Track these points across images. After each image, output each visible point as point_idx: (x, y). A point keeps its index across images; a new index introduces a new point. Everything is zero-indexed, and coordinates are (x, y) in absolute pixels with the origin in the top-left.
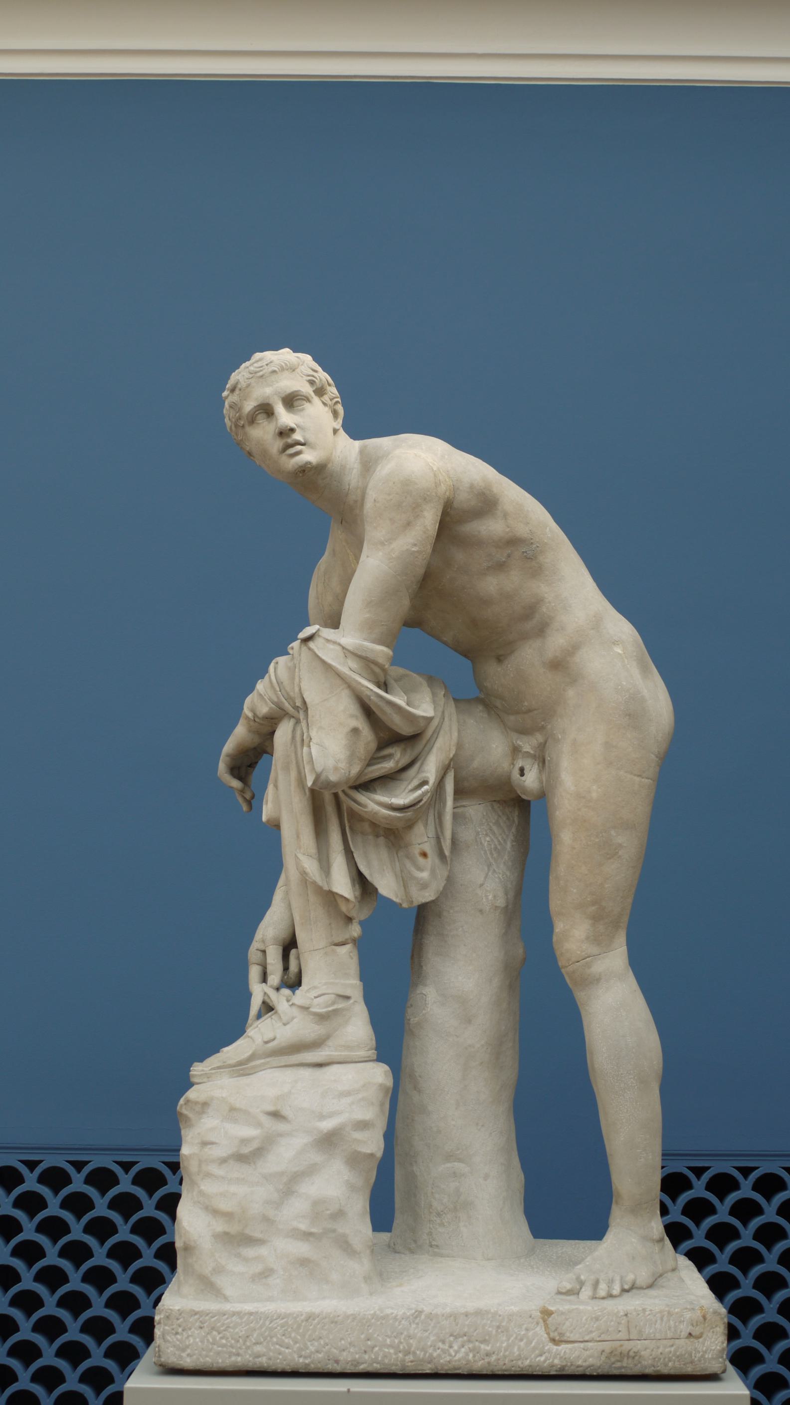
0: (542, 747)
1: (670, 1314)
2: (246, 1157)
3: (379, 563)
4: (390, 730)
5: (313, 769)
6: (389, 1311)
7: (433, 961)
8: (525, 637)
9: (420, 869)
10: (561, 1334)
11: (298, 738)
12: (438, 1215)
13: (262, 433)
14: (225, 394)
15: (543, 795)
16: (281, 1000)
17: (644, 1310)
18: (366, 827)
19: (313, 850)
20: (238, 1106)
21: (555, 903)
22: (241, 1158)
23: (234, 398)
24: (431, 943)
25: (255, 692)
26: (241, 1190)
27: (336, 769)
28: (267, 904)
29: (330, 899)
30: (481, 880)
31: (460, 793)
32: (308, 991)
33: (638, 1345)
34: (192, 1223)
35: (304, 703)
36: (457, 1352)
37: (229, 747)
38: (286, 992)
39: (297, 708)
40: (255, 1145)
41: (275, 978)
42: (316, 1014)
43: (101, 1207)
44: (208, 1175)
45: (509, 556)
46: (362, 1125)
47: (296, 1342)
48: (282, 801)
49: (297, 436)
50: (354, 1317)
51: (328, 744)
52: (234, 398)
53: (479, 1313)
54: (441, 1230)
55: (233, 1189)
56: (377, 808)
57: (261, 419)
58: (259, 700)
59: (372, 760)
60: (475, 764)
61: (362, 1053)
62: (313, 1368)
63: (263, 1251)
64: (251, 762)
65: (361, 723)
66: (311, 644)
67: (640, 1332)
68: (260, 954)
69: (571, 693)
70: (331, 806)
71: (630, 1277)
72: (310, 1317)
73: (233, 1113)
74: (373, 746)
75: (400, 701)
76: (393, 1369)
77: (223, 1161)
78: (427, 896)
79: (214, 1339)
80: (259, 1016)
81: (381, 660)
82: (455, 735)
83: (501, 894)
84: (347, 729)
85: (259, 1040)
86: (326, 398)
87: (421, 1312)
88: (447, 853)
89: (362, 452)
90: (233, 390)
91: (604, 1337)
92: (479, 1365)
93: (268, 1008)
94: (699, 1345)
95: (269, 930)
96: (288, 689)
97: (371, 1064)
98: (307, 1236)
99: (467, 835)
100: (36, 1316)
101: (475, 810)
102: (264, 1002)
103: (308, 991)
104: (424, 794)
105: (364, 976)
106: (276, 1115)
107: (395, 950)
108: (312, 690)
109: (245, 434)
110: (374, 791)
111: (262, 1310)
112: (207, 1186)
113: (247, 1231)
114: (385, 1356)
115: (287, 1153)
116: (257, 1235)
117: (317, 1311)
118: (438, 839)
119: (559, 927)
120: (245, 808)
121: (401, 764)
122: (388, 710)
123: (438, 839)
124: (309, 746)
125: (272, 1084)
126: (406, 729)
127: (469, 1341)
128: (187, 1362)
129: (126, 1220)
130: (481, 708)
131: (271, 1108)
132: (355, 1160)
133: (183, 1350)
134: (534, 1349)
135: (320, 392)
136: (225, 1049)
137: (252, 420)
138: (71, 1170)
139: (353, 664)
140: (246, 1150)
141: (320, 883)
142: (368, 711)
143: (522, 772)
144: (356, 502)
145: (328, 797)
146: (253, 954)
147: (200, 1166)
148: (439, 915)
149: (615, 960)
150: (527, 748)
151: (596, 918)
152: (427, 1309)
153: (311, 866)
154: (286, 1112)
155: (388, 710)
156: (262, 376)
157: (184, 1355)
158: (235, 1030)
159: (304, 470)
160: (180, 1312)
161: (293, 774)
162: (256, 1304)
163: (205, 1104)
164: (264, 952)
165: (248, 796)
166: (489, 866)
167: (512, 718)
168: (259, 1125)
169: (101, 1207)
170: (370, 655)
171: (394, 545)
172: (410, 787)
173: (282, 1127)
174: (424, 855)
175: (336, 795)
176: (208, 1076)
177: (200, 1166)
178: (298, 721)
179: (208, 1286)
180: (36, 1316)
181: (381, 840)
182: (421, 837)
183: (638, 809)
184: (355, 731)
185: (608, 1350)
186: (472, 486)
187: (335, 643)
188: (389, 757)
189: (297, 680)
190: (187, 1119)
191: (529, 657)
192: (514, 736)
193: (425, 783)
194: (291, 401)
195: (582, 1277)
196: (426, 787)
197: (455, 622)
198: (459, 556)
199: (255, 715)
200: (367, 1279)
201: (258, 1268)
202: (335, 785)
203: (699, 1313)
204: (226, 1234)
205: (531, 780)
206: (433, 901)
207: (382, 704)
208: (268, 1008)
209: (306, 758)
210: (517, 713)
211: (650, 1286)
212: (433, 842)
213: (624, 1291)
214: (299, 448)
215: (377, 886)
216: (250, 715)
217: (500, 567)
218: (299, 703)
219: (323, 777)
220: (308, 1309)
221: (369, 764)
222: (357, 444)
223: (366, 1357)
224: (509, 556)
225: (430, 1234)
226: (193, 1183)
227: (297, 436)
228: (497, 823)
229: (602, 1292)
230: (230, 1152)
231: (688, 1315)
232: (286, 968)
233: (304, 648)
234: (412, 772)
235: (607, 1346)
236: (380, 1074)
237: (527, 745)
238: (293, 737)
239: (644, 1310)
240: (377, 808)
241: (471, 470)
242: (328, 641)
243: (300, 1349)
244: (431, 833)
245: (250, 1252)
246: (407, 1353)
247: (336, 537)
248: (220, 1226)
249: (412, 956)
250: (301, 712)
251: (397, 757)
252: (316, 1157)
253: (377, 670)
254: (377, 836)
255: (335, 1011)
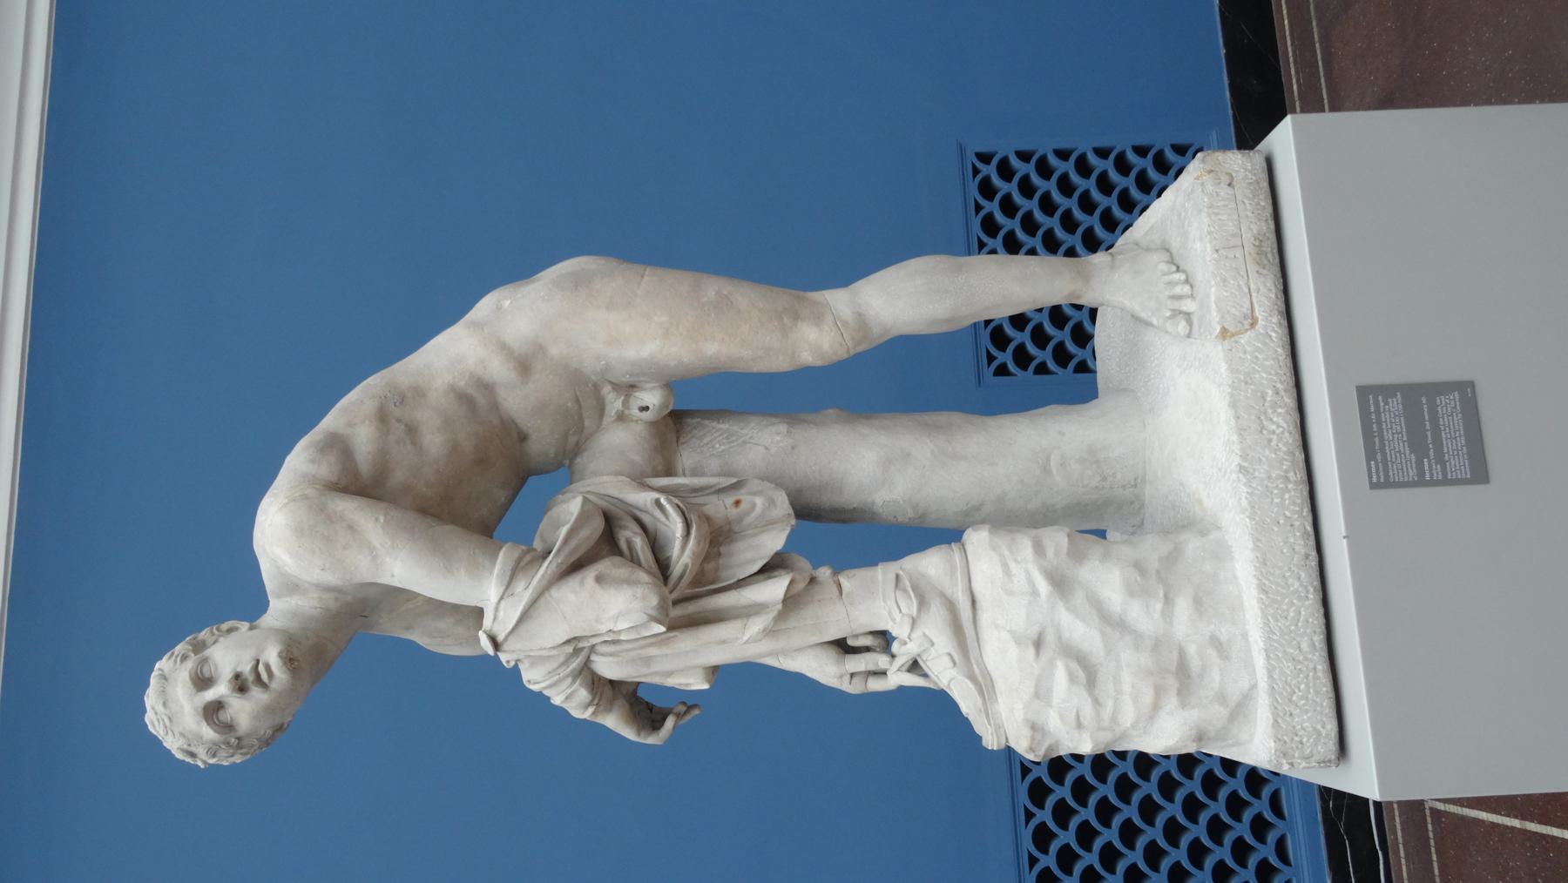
0: (617, 387)
1: (1210, 207)
2: (1088, 673)
3: (399, 562)
4: (598, 543)
5: (643, 625)
6: (1244, 502)
7: (849, 497)
8: (495, 406)
9: (754, 506)
10: (1245, 317)
11: (611, 649)
12: (1104, 479)
13: (243, 711)
14: (200, 764)
15: (674, 384)
16: (904, 650)
17: (1210, 233)
18: (709, 567)
19: (738, 624)
20: (1032, 690)
21: (781, 364)
22: (1091, 682)
23: (201, 752)
24: (829, 500)
25: (546, 693)
26: (1127, 679)
27: (644, 598)
28: (799, 678)
29: (791, 602)
30: (762, 449)
31: (669, 472)
32: (894, 621)
33: (1248, 238)
34: (1164, 737)
35: (568, 642)
36: (1279, 426)
37: (629, 733)
38: (895, 647)
39: (577, 651)
40: (1075, 666)
41: (882, 661)
42: (919, 610)
43: (1067, 837)
44: (1114, 719)
45: (399, 421)
46: (1039, 548)
47: (1292, 604)
48: (684, 664)
49: (246, 669)
50: (1256, 540)
51: (613, 609)
52: (201, 752)
53: (1234, 404)
54: (1119, 476)
55: (1126, 687)
56: (688, 552)
57: (225, 716)
58: (573, 700)
59: (634, 560)
60: (637, 458)
61: (957, 556)
62: (1317, 583)
63: (1192, 650)
64: (645, 706)
65: (589, 574)
66: (500, 638)
67: (1233, 235)
68: (855, 680)
69: (555, 351)
70: (688, 601)
71: (1163, 267)
72: (1262, 589)
73: (1041, 693)
74: (617, 559)
75: (564, 531)
76: (1306, 493)
77: (1096, 702)
78: (783, 506)
79: (1301, 698)
80: (925, 676)
81: (516, 554)
82: (605, 478)
83: (774, 429)
84: (597, 588)
85: (953, 672)
86: (210, 640)
87: (1241, 467)
88: (734, 480)
89: (279, 597)
90: (193, 755)
91: (1243, 272)
92: (1289, 401)
93: (914, 666)
94: (1239, 175)
95: (825, 670)
96: (555, 665)
97: (969, 547)
98: (1168, 600)
99: (714, 465)
100: (1102, 872)
101: (687, 457)
102: (909, 671)
103: (894, 621)
104: (670, 502)
105: (873, 563)
106: (1038, 644)
107: (839, 534)
108: (552, 631)
109: (248, 735)
110: (669, 559)
111: (1262, 645)
112: (1128, 717)
113: (1173, 668)
114: (1294, 503)
115: (1081, 631)
116: (1175, 656)
117: (1255, 581)
118: (720, 491)
119: (807, 358)
120: (696, 712)
121: (637, 529)
122: (573, 543)
123: (720, 491)
124: (620, 632)
125: (1001, 653)
126: (598, 525)
127: (1265, 413)
128: (1331, 727)
129: (1076, 812)
130: (578, 460)
131: (1032, 650)
132: (1077, 555)
133: (1319, 734)
134: (1265, 344)
135: (199, 647)
136: (964, 710)
137: (228, 727)
138: (1038, 868)
139: (519, 586)
140: (1081, 675)
141: (774, 614)
142: (576, 566)
143: (645, 409)
144: (337, 599)
145: (676, 612)
146: (854, 688)
147: (1104, 729)
148: (800, 491)
149: (838, 300)
150: (618, 404)
151: (796, 317)
152: (1237, 460)
153: (756, 625)
154: (1033, 632)
155: (573, 543)
156: (170, 719)
157: (1324, 732)
158: (941, 701)
159: (289, 660)
160: (1277, 740)
161: (653, 651)
162: (1255, 653)
163: (1034, 727)
164: (852, 675)
165: (682, 708)
166: (745, 443)
167: (587, 423)
168: (1051, 664)
169: (1067, 837)
170: (509, 568)
171: (377, 544)
172: (663, 518)
173: (1050, 638)
174: (737, 503)
175: (675, 603)
176: (998, 727)
177: (1104, 729)
178: (592, 649)
179: (1240, 710)
180: (1102, 872)
181: (723, 549)
182: (720, 507)
183: (676, 283)
184: (599, 579)
185: (1257, 268)
186: (313, 461)
187: (497, 609)
188: (629, 543)
189: (543, 653)
190: (1050, 748)
191: (517, 401)
192: (607, 420)
193: (658, 503)
194: (202, 682)
195: (1168, 314)
196: (663, 501)
197: (489, 485)
198: (399, 476)
199: (590, 704)
200: (1203, 533)
201: (1212, 653)
202: (663, 599)
203: (1206, 177)
204: (1179, 693)
205: (652, 397)
206: (789, 495)
207: (567, 550)
208: (914, 666)
209: (633, 636)
210: (581, 419)
211: (1168, 250)
212: (722, 496)
213: (1178, 270)
214: (261, 668)
215: (772, 553)
216: (591, 710)
217: (412, 430)
218: (570, 649)
219: (653, 613)
220: (1254, 592)
221: (640, 565)
222: (273, 602)
223: (1297, 524)
224: (399, 421)
225: (1124, 487)
226: (1124, 736)
227: (246, 669)
228: (700, 439)
229: (1187, 289)
230: (1086, 695)
231: (1210, 188)
232: (867, 649)
233: (505, 647)
234: (646, 519)
235: (1252, 268)
236: (977, 539)
237: (614, 404)
238: (611, 655)
239: (1210, 233)
240: (688, 552)
241: (299, 461)
242: (495, 618)
243: (1300, 598)
244: (714, 498)
245: (1195, 664)
246: (1287, 479)
247: (391, 627)
248: (1172, 701)
249: (844, 521)
250: (580, 645)
251: (631, 536)
252: (1079, 598)
253: (528, 558)
254: (719, 554)
255: (915, 588)
